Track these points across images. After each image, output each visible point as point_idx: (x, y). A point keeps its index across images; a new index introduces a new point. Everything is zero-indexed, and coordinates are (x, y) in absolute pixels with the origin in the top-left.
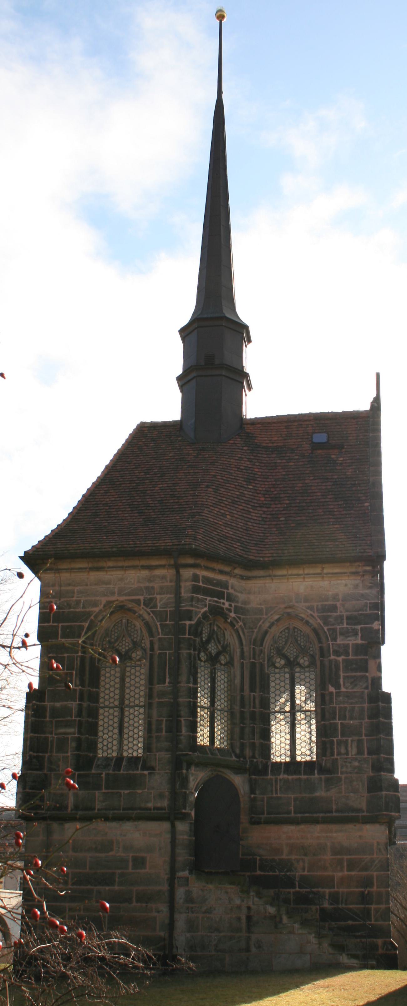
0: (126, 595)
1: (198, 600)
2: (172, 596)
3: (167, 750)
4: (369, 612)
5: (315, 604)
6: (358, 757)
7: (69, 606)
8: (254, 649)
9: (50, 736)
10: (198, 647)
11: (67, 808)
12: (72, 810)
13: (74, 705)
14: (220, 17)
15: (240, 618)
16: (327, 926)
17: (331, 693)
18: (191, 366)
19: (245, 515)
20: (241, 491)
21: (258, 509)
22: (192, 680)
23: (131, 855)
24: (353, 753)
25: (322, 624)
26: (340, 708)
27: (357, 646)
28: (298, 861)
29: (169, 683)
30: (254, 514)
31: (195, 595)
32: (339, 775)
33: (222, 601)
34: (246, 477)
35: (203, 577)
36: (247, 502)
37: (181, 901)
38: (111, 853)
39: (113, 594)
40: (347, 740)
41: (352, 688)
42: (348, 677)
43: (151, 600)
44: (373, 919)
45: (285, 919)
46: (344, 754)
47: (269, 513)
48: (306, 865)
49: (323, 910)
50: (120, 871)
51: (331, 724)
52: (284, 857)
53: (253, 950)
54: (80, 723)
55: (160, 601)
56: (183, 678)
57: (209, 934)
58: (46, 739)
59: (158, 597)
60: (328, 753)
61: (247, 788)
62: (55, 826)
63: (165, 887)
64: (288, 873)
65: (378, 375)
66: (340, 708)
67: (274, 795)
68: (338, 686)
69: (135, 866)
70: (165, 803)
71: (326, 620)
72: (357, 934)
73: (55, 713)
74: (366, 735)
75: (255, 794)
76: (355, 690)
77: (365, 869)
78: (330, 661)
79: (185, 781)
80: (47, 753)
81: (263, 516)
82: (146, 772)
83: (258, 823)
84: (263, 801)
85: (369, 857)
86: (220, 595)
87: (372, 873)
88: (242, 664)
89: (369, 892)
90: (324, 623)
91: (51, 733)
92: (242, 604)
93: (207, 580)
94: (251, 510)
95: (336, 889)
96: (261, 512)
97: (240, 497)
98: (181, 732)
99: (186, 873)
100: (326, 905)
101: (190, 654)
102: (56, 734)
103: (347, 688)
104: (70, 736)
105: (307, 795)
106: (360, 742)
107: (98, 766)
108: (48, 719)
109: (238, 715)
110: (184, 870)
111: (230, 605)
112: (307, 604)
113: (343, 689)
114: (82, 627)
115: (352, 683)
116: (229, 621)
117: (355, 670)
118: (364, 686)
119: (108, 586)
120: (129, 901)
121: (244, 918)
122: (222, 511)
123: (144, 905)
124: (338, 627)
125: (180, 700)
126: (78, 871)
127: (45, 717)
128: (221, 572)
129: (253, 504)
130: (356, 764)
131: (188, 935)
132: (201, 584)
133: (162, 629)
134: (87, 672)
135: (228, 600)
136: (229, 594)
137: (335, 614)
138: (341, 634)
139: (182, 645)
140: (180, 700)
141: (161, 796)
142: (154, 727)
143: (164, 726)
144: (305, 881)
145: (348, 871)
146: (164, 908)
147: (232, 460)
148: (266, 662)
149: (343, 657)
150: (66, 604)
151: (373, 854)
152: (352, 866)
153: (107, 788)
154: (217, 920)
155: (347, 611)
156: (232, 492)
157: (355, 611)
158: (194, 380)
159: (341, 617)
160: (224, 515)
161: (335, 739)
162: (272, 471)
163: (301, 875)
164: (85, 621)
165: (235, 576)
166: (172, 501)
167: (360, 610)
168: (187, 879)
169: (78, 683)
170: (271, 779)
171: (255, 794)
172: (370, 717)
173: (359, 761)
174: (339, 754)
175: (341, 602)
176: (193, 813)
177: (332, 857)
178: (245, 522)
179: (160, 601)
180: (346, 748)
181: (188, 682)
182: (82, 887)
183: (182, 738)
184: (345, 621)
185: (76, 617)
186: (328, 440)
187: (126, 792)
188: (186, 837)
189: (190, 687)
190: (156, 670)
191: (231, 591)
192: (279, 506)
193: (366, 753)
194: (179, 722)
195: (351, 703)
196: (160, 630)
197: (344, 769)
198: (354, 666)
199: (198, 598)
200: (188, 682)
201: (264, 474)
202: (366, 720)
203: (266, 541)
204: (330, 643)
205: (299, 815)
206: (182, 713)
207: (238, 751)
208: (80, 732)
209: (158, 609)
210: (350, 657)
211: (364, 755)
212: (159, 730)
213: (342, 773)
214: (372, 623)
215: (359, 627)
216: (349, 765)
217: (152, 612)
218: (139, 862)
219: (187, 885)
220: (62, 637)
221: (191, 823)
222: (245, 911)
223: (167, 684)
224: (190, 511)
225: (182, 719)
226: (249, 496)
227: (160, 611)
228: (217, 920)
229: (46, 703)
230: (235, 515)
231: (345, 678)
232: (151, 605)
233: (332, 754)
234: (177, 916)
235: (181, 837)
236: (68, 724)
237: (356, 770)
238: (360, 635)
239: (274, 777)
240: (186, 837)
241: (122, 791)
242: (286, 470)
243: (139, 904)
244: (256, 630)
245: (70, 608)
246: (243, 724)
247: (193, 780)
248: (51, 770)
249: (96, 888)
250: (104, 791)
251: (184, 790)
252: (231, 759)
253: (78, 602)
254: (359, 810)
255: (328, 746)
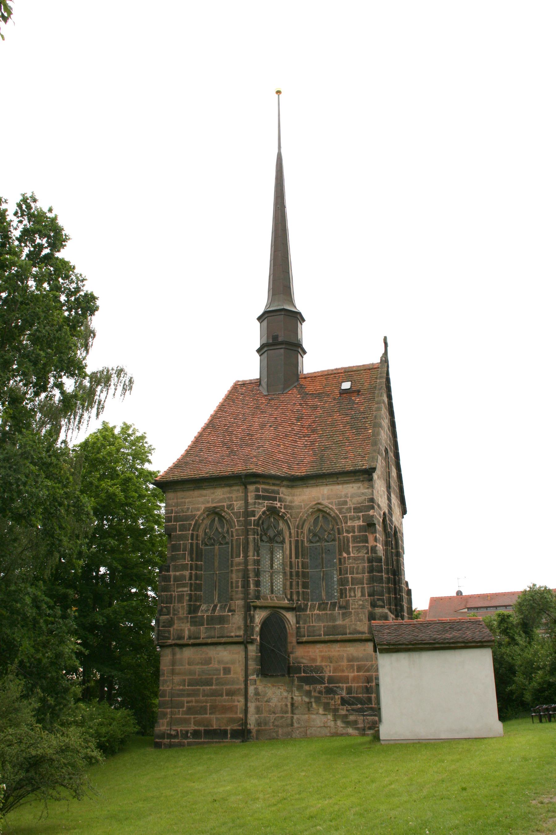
0: (216, 503)
1: (259, 503)
2: (243, 502)
3: (242, 599)
4: (367, 504)
5: (334, 501)
6: (362, 598)
7: (183, 511)
8: (297, 531)
9: (173, 593)
10: (259, 533)
11: (184, 638)
12: (187, 639)
13: (187, 573)
14: (278, 92)
15: (288, 512)
16: (345, 708)
17: (345, 557)
18: (263, 344)
19: (293, 444)
20: (292, 427)
21: (303, 438)
22: (256, 554)
23: (222, 666)
24: (359, 596)
25: (338, 514)
26: (350, 567)
27: (360, 527)
28: (326, 666)
29: (243, 557)
30: (299, 443)
31: (257, 501)
32: (351, 610)
33: (275, 502)
34: (296, 417)
35: (262, 488)
36: (295, 435)
37: (252, 695)
38: (211, 665)
39: (208, 502)
40: (355, 588)
41: (357, 554)
42: (354, 547)
43: (231, 505)
44: (373, 704)
45: (314, 705)
46: (353, 597)
47: (309, 441)
48: (332, 669)
49: (342, 699)
50: (215, 677)
51: (345, 577)
52: (318, 664)
53: (296, 725)
54: (191, 584)
55: (236, 505)
56: (251, 553)
57: (268, 715)
58: (171, 595)
59: (235, 503)
60: (344, 596)
61: (295, 621)
62: (177, 649)
63: (242, 686)
64: (321, 675)
65: (385, 339)
66: (350, 567)
67: (311, 624)
68: (348, 553)
69: (225, 673)
70: (241, 633)
71: (340, 510)
72: (365, 713)
73: (176, 579)
74: (367, 584)
75: (299, 624)
76: (359, 555)
77: (368, 670)
78: (344, 537)
79: (252, 619)
80: (172, 603)
81: (305, 443)
82: (230, 614)
83: (301, 643)
84: (304, 628)
85: (370, 663)
86: (274, 499)
87: (372, 673)
88: (290, 541)
89: (370, 685)
90: (340, 513)
91: (174, 591)
92: (289, 503)
93: (265, 490)
94: (298, 440)
95: (350, 684)
96: (304, 441)
97: (291, 432)
98: (250, 587)
99: (255, 677)
100: (344, 694)
101: (254, 538)
102: (177, 592)
103: (354, 554)
104: (185, 593)
105: (331, 624)
106: (363, 588)
107: (202, 611)
108: (172, 583)
109: (289, 574)
110: (253, 675)
111: (281, 505)
112: (329, 501)
113: (352, 555)
114: (190, 524)
115: (357, 550)
116: (281, 514)
117: (359, 542)
118: (365, 552)
119: (205, 498)
120: (221, 695)
121: (289, 705)
122: (278, 443)
123: (230, 698)
124: (348, 515)
125: (249, 567)
126: (191, 677)
127: (170, 582)
128: (274, 485)
129: (299, 436)
130: (361, 603)
131: (257, 716)
132: (261, 493)
133: (237, 523)
134: (195, 552)
135: (279, 501)
136: (280, 498)
137: (346, 507)
138: (350, 519)
139: (250, 533)
140: (249, 567)
141: (239, 628)
142: (234, 585)
143: (240, 584)
144: (331, 680)
145: (357, 672)
146: (242, 699)
147: (289, 406)
148: (305, 539)
149: (351, 534)
150: (181, 510)
151: (373, 661)
152: (359, 669)
153: (207, 625)
154: (274, 706)
155: (354, 504)
156: (286, 428)
157: (359, 504)
158: (266, 353)
159: (350, 508)
160: (279, 446)
161: (347, 587)
162: (314, 411)
163: (329, 676)
164: (192, 520)
165: (283, 486)
166: (248, 438)
167: (362, 503)
168: (255, 681)
169: (189, 559)
170: (309, 614)
171: (299, 624)
172: (368, 572)
173: (363, 601)
174: (350, 596)
175: (349, 498)
176: (258, 639)
177: (348, 663)
178: (293, 449)
179: (236, 505)
180: (354, 592)
181: (254, 556)
182: (194, 688)
183: (251, 591)
184: (352, 511)
185: (187, 518)
186: (351, 386)
187: (218, 626)
188: (254, 654)
189: (255, 559)
190: (235, 549)
191: (281, 495)
192: (316, 435)
193: (367, 595)
194: (248, 582)
195: (357, 564)
196: (236, 524)
197: (353, 606)
198: (358, 539)
199: (259, 502)
200: (254, 556)
201: (309, 413)
202: (367, 574)
203: (304, 461)
204: (344, 525)
205: (327, 637)
206: (251, 575)
207: (289, 597)
208: (191, 590)
209: (235, 511)
210: (356, 534)
211: (366, 597)
212: (237, 587)
213: (352, 609)
214: (369, 512)
215: (361, 514)
216: (356, 603)
217: (232, 512)
218: (227, 671)
219: (256, 684)
220: (179, 532)
221: (257, 645)
222: (290, 700)
223: (241, 558)
224: (257, 445)
225: (251, 579)
226: (297, 430)
227: (237, 512)
228: (274, 706)
229: (171, 573)
230: (286, 445)
231: (353, 547)
232: (231, 508)
233: (346, 597)
234: (249, 704)
235: (251, 654)
236: (184, 586)
237: (361, 607)
238: (362, 519)
239: (311, 613)
240: (254, 654)
241: (216, 626)
242: (323, 410)
243: (227, 697)
244: (298, 519)
245: (184, 513)
246: (292, 579)
247: (258, 617)
248: (174, 614)
249: (201, 688)
250: (205, 626)
251: (252, 624)
252: (284, 602)
253: (188, 509)
254: (363, 633)
255: (344, 591)
